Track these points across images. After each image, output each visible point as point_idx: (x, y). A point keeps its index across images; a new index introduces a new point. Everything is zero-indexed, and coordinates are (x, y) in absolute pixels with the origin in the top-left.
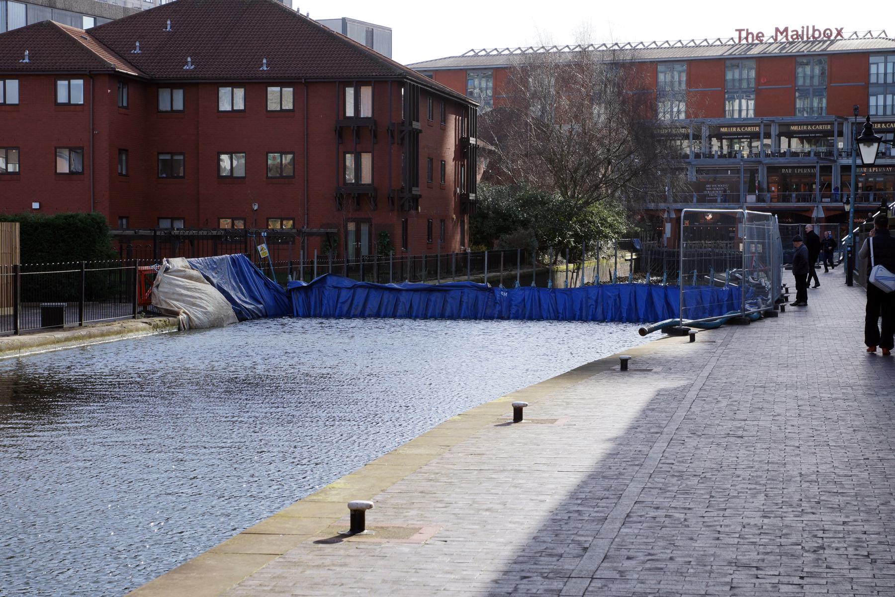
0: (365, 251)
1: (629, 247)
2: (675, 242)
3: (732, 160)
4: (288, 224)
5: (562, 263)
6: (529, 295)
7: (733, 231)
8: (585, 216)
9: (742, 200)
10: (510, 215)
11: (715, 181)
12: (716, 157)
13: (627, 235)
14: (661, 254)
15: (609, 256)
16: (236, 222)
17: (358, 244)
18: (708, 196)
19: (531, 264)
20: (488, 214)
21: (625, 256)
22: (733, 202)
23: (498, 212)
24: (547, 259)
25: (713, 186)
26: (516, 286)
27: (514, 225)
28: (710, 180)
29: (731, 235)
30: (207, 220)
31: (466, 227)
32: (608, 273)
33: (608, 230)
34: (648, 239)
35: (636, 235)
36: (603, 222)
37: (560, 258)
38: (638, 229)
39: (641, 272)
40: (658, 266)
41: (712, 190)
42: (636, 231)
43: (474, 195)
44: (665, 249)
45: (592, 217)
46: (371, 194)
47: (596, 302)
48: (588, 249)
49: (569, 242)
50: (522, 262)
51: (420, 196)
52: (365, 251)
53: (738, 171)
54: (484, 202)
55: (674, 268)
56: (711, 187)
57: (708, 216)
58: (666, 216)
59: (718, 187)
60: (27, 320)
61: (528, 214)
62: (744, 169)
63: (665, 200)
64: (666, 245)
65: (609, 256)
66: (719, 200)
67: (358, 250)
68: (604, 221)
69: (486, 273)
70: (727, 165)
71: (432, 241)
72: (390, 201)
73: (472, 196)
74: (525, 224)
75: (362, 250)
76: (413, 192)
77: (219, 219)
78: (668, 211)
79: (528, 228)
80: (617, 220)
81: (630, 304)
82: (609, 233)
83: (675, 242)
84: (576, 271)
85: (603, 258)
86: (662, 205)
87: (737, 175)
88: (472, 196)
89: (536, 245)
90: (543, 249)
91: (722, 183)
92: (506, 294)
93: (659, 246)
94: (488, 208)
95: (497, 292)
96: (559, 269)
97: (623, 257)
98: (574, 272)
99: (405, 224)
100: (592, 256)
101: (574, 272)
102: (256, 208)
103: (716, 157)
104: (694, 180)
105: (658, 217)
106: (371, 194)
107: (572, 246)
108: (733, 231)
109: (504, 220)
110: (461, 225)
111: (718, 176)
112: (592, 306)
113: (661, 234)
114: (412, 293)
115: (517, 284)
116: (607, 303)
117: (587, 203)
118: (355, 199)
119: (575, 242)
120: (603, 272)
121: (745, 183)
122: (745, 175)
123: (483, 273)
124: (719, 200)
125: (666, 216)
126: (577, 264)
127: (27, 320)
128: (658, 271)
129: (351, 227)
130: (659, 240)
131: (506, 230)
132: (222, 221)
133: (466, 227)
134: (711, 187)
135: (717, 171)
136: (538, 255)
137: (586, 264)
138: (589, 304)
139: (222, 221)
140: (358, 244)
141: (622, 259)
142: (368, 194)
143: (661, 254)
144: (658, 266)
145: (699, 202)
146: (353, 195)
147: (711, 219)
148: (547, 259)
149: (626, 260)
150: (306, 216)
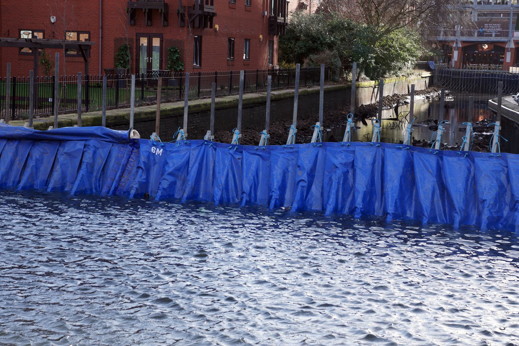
0: (156, 67)
1: (427, 68)
2: (460, 65)
3: (505, 6)
4: (84, 37)
5: (364, 79)
6: (197, 157)
7: (503, 58)
8: (387, 41)
9: (510, 35)
10: (319, 39)
11: (491, 22)
12: (493, 4)
13: (421, 59)
14: (449, 73)
15: (408, 74)
16: (81, 35)
17: (149, 59)
18: (486, 32)
19: (334, 81)
20: (300, 36)
21: (422, 74)
22: (503, 36)
23: (308, 35)
24: (350, 77)
25: (489, 25)
26: (179, 138)
27: (322, 46)
28: (488, 21)
29: (501, 60)
30: (9, 31)
31: (275, 46)
32: (407, 88)
33: (406, 54)
34: (441, 61)
35: (431, 58)
36: (402, 47)
37: (363, 75)
38: (432, 54)
39: (433, 86)
40: (446, 82)
41: (489, 28)
42: (430, 55)
43: (283, 18)
44: (453, 70)
45: (392, 42)
46: (162, 10)
47: (311, 175)
48: (389, 68)
49: (371, 62)
50: (326, 78)
51: (214, 14)
52: (156, 67)
53: (508, 14)
54: (298, 26)
55: (459, 84)
56: (488, 26)
57: (485, 46)
58: (454, 45)
59: (493, 26)
60: (69, 96)
61: (334, 37)
62: (513, 13)
63: (454, 34)
64: (453, 66)
65: (408, 74)
66: (494, 35)
67: (150, 65)
68: (402, 46)
69: (296, 85)
70: (500, 10)
71: (233, 59)
72: (180, 16)
73: (280, 19)
74: (331, 46)
75: (153, 65)
76: (205, 10)
77: (20, 30)
78: (456, 42)
79: (333, 50)
80: (413, 46)
81: (372, 182)
82: (406, 56)
83: (460, 65)
84: (377, 87)
85: (403, 76)
86: (451, 38)
87: (507, 17)
88: (280, 19)
89: (339, 64)
90: (349, 68)
91: (497, 23)
92: (159, 152)
93: (448, 68)
94: (301, 31)
95: (143, 148)
96: (360, 85)
97: (419, 75)
98: (375, 87)
99: (199, 41)
100: (393, 74)
101: (375, 87)
102: (53, 20)
103: (493, 4)
104: (476, 20)
105: (448, 46)
106: (162, 10)
107: (373, 66)
108: (503, 58)
109: (313, 42)
110: (269, 45)
111: (493, 17)
112: (301, 184)
113: (450, 58)
114: (5, 142)
115: (182, 133)
116: (330, 179)
117: (388, 31)
118: (162, 14)
119: (375, 63)
120: (402, 87)
121: (513, 23)
122: (513, 18)
123: (136, 115)
124: (494, 35)
125: (454, 45)
126: (378, 81)
127: (69, 96)
128: (446, 86)
129: (144, 41)
130: (448, 63)
131: (315, 50)
132: (22, 32)
133: (275, 46)
134: (488, 26)
135: (493, 14)
136: (341, 73)
137: (387, 81)
138: (298, 179)
139: (22, 32)
140: (149, 59)
141: (419, 77)
142: (158, 9)
143: (449, 73)
144: (447, 82)
145: (479, 36)
146: (144, 11)
147: (487, 48)
148: (350, 77)
149: (422, 77)
150: (101, 30)
